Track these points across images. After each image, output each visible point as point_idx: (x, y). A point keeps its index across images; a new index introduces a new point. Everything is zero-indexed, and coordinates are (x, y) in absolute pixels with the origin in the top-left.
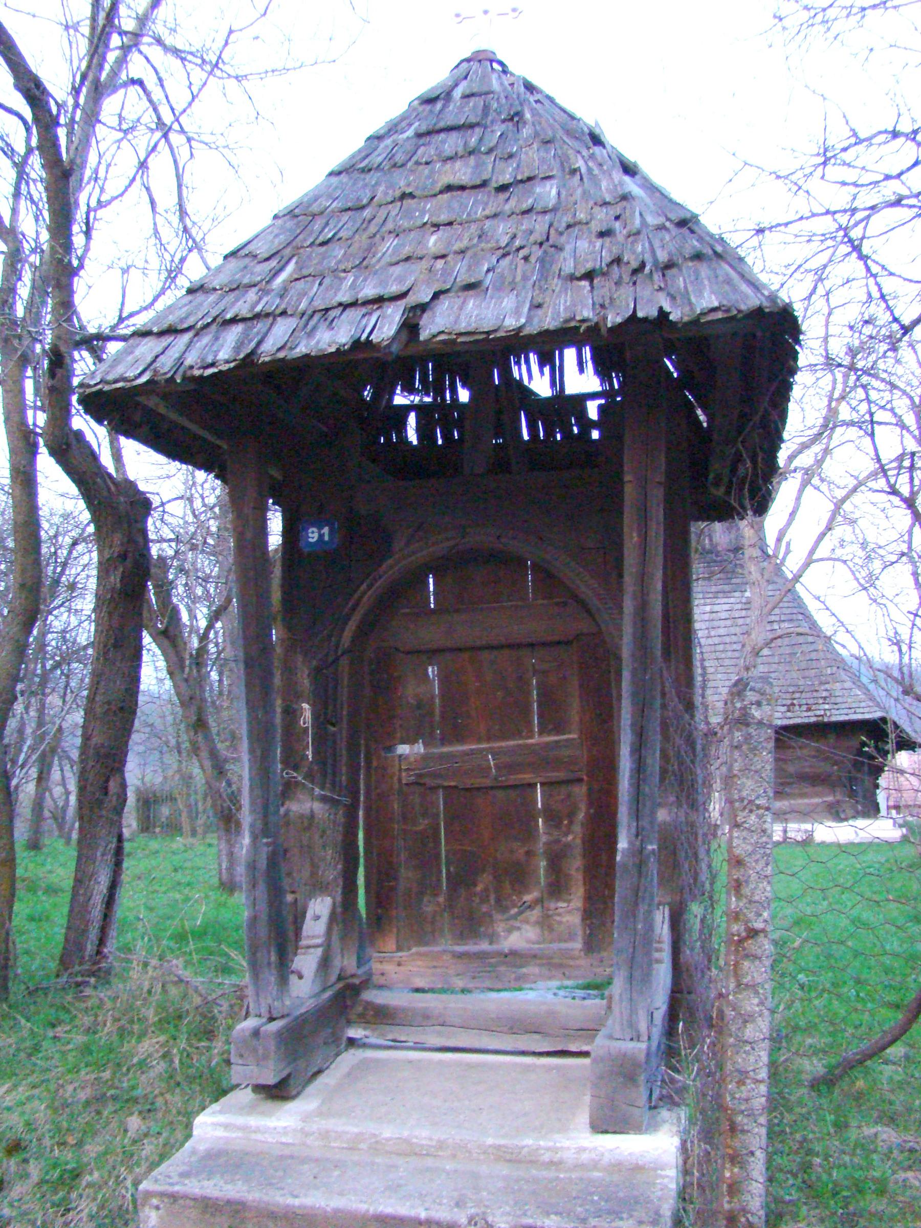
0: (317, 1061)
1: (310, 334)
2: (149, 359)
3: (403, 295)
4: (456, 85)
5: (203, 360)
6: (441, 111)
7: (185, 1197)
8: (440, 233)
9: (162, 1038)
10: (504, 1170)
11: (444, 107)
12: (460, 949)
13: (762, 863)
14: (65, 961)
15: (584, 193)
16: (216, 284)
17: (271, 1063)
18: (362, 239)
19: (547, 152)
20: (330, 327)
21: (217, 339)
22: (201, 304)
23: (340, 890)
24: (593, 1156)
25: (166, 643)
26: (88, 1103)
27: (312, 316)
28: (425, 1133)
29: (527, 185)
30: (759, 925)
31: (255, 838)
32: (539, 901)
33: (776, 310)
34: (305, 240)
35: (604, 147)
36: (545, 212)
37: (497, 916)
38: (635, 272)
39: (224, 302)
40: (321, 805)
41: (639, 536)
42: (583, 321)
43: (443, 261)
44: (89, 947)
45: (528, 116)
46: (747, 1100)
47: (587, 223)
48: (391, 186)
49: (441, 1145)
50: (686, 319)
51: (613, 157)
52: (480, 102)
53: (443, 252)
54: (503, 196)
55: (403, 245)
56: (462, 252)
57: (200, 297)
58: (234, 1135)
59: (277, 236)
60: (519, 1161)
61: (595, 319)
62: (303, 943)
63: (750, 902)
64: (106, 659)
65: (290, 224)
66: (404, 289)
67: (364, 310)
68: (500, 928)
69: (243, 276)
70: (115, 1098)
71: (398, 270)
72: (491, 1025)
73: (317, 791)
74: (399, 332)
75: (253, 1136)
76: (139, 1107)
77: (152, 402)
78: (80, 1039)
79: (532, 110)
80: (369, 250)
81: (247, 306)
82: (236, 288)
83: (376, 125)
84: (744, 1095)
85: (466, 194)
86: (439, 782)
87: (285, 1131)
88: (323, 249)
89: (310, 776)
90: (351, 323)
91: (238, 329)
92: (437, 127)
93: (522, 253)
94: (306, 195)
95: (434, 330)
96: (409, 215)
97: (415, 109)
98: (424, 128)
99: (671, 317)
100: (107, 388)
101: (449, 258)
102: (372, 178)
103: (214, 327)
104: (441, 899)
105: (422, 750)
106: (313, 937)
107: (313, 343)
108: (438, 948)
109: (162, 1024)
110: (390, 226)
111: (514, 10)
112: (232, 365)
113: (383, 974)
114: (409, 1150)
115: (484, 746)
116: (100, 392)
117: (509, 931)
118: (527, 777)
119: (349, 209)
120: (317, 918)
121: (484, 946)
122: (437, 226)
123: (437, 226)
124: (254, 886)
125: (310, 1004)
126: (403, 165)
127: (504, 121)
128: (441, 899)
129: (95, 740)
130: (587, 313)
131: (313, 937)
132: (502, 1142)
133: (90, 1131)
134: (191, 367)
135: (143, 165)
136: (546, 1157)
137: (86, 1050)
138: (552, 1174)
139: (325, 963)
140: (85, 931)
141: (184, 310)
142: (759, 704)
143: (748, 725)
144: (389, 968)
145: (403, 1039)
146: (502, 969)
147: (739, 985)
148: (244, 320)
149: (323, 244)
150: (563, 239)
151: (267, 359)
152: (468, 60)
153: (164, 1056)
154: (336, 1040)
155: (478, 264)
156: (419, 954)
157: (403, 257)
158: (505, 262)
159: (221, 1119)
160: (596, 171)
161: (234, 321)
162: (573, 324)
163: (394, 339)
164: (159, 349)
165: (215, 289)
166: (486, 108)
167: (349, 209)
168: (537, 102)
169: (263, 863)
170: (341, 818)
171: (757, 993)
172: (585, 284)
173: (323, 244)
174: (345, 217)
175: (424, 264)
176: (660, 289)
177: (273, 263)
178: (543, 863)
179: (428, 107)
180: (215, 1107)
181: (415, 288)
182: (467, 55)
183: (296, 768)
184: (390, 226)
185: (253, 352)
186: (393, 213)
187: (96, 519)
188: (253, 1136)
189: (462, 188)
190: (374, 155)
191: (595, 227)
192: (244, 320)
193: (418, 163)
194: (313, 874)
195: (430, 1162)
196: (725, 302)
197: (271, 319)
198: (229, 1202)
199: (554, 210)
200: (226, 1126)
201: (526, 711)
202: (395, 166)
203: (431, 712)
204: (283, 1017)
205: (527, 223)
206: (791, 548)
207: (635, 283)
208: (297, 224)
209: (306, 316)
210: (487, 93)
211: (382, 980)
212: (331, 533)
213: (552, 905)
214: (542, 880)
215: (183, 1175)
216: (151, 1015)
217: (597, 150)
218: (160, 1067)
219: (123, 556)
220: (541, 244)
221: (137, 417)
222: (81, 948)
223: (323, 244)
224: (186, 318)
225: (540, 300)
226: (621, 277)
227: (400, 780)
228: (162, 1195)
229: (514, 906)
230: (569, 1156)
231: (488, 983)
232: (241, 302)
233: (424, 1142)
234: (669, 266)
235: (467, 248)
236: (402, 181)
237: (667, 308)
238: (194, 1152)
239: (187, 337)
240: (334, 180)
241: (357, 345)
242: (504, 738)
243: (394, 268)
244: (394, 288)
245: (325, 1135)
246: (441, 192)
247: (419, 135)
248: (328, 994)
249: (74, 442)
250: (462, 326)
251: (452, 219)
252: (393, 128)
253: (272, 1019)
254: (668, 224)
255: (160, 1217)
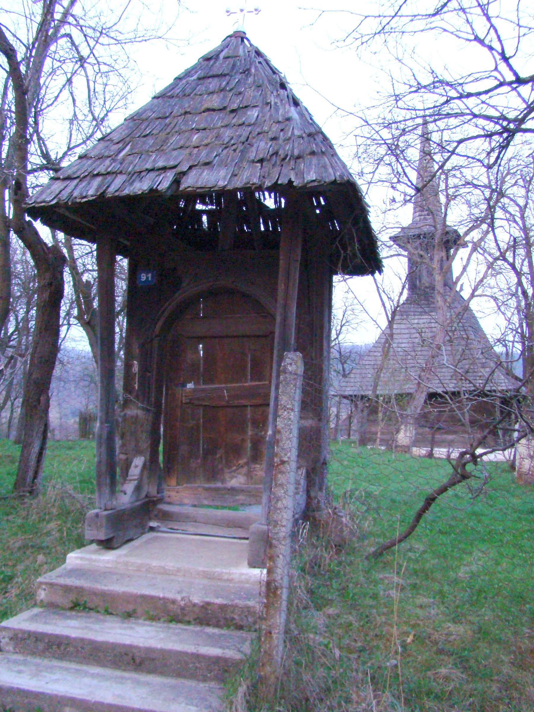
0: (131, 533)
1: (132, 184)
2: (57, 192)
3: (175, 167)
4: (222, 51)
5: (81, 194)
6: (212, 65)
7: (57, 585)
8: (199, 134)
9: (59, 522)
10: (205, 581)
11: (215, 63)
12: (207, 485)
13: (288, 433)
14: (17, 485)
15: (271, 115)
16: (92, 155)
17: (103, 530)
18: (163, 135)
19: (258, 92)
20: (141, 180)
21: (89, 183)
22: (84, 165)
23: (148, 454)
24: (247, 577)
25: (89, 329)
26: (20, 548)
27: (133, 175)
28: (172, 564)
29: (244, 110)
30: (286, 459)
31: (102, 423)
32: (247, 464)
33: (343, 181)
34: (137, 133)
35: (286, 90)
36: (249, 125)
37: (226, 470)
38: (284, 159)
39: (95, 165)
40: (142, 412)
41: (285, 285)
42: (253, 184)
43: (197, 149)
44: (28, 480)
45: (253, 70)
46: (277, 533)
47: (267, 133)
48: (181, 107)
49: (178, 570)
50: (300, 185)
51: (290, 97)
52: (231, 61)
53: (198, 145)
54: (232, 115)
55: (180, 140)
56: (207, 145)
57: (84, 161)
58: (85, 563)
59: (124, 130)
60: (214, 579)
61: (260, 183)
62: (129, 478)
63: (282, 449)
64: (41, 336)
65: (131, 124)
66: (176, 164)
67: (157, 173)
68: (227, 476)
69: (105, 152)
70: (33, 547)
71: (175, 153)
72: (218, 523)
73: (140, 405)
74: (171, 185)
75: (93, 563)
76: (44, 551)
77: (62, 211)
78: (19, 521)
79: (256, 67)
80: (164, 141)
81: (105, 167)
82: (101, 158)
83: (179, 71)
84: (276, 531)
85: (214, 113)
86: (200, 403)
87: (108, 562)
88: (145, 139)
89: (137, 397)
90: (150, 179)
91: (99, 179)
92: (208, 75)
93: (234, 147)
94: (141, 108)
95: (186, 186)
96: (186, 122)
97: (200, 63)
98: (202, 75)
99: (294, 184)
100: (37, 205)
101: (200, 148)
102: (173, 102)
103: (88, 178)
104: (199, 461)
105: (193, 387)
106: (134, 475)
107: (132, 189)
108: (197, 485)
109: (59, 516)
110: (177, 129)
111: (256, 10)
112: (94, 198)
113: (169, 497)
114: (164, 572)
115: (223, 385)
116: (34, 207)
117: (232, 478)
118: (244, 402)
119: (160, 118)
120: (136, 466)
121: (219, 485)
122: (198, 130)
123: (198, 130)
124: (101, 447)
125: (129, 506)
126: (189, 95)
127: (241, 73)
128: (199, 461)
129: (34, 376)
130: (255, 181)
131: (134, 475)
132: (206, 569)
133: (19, 560)
134: (76, 198)
135: (69, 81)
136: (226, 577)
137: (21, 526)
138: (227, 584)
139: (138, 489)
140: (27, 472)
141: (76, 167)
142: (291, 364)
143: (286, 373)
144: (173, 494)
145: (176, 528)
146: (227, 496)
147: (276, 485)
148: (102, 175)
149: (145, 136)
150: (254, 140)
151: (110, 196)
152: (230, 36)
153: (59, 531)
154: (143, 526)
155: (211, 151)
156: (186, 487)
157: (179, 146)
158: (225, 152)
159: (80, 555)
160: (279, 104)
161: (98, 175)
162: (249, 185)
163: (169, 188)
164: (62, 187)
165: (91, 158)
166: (234, 66)
167: (160, 118)
168: (260, 63)
169: (105, 436)
170: (151, 417)
171: (283, 488)
172: (259, 165)
173: (145, 136)
174: (157, 122)
175: (187, 151)
176: (292, 169)
177: (120, 145)
178: (249, 445)
179: (206, 63)
180: (78, 551)
181: (181, 164)
182: (231, 33)
183: (130, 393)
184: (177, 129)
185: (104, 192)
186: (179, 122)
187: (37, 265)
188: (93, 563)
189: (214, 110)
190: (176, 89)
191: (271, 135)
192: (102, 175)
193: (195, 94)
194: (136, 446)
195: (173, 577)
196: (318, 178)
197: (115, 175)
198: (76, 587)
199: (254, 124)
200: (82, 558)
201: (244, 368)
202: (185, 95)
203: (199, 368)
204: (112, 509)
205: (240, 131)
206: (464, 288)
207: (282, 166)
208: (135, 124)
209: (131, 175)
210: (236, 57)
211: (168, 500)
212: (152, 277)
213: (253, 466)
214: (249, 453)
215: (58, 576)
216: (54, 511)
217: (282, 92)
218: (58, 535)
219: (50, 284)
220: (243, 143)
221: (55, 218)
222: (25, 479)
223: (145, 136)
224: (76, 172)
225: (236, 172)
226: (276, 162)
227: (182, 401)
228: (46, 584)
229: (235, 465)
230: (236, 577)
231: (219, 503)
232: (102, 166)
233: (171, 568)
234: (299, 157)
235: (209, 144)
236: (187, 104)
237: (293, 180)
238: (65, 569)
239: (76, 182)
240: (156, 101)
241: (152, 191)
242: (232, 382)
243: (174, 152)
244: (172, 163)
245: (126, 564)
246: (204, 112)
247: (199, 79)
248: (137, 503)
249: (27, 227)
250: (199, 184)
251: (206, 127)
252: (188, 73)
253: (106, 510)
254: (304, 135)
255: (46, 594)
